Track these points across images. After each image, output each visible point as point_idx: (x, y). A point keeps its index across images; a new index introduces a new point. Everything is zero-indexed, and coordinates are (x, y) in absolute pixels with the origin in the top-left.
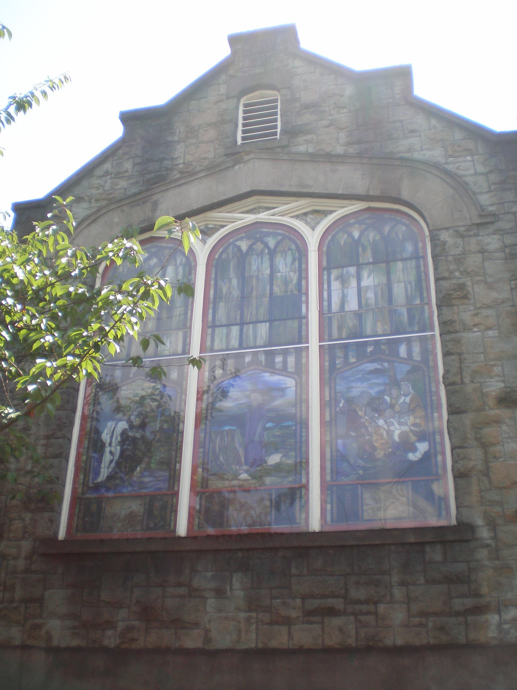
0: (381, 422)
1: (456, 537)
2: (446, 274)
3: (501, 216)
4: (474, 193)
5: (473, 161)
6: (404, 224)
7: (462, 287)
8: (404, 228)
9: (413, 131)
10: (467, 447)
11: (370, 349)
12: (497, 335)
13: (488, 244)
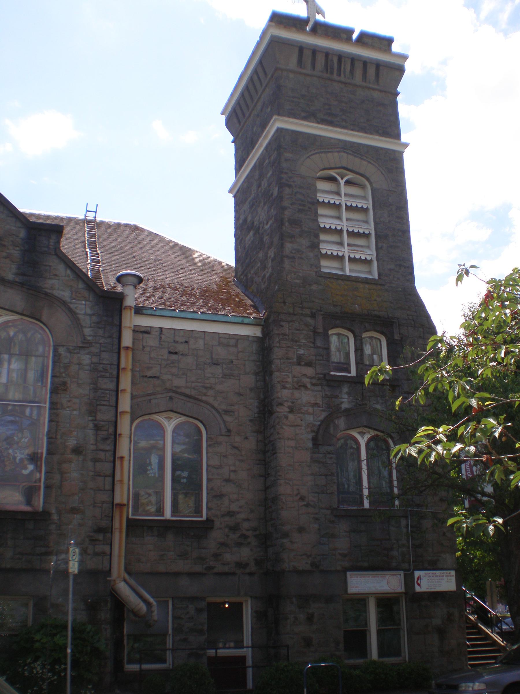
0: (10, 451)
1: (40, 518)
2: (58, 374)
3: (93, 344)
4: (82, 326)
5: (85, 305)
6: (40, 334)
7: (65, 384)
8: (39, 336)
9: (56, 275)
10: (52, 473)
11: (10, 408)
12: (78, 414)
13: (84, 360)
